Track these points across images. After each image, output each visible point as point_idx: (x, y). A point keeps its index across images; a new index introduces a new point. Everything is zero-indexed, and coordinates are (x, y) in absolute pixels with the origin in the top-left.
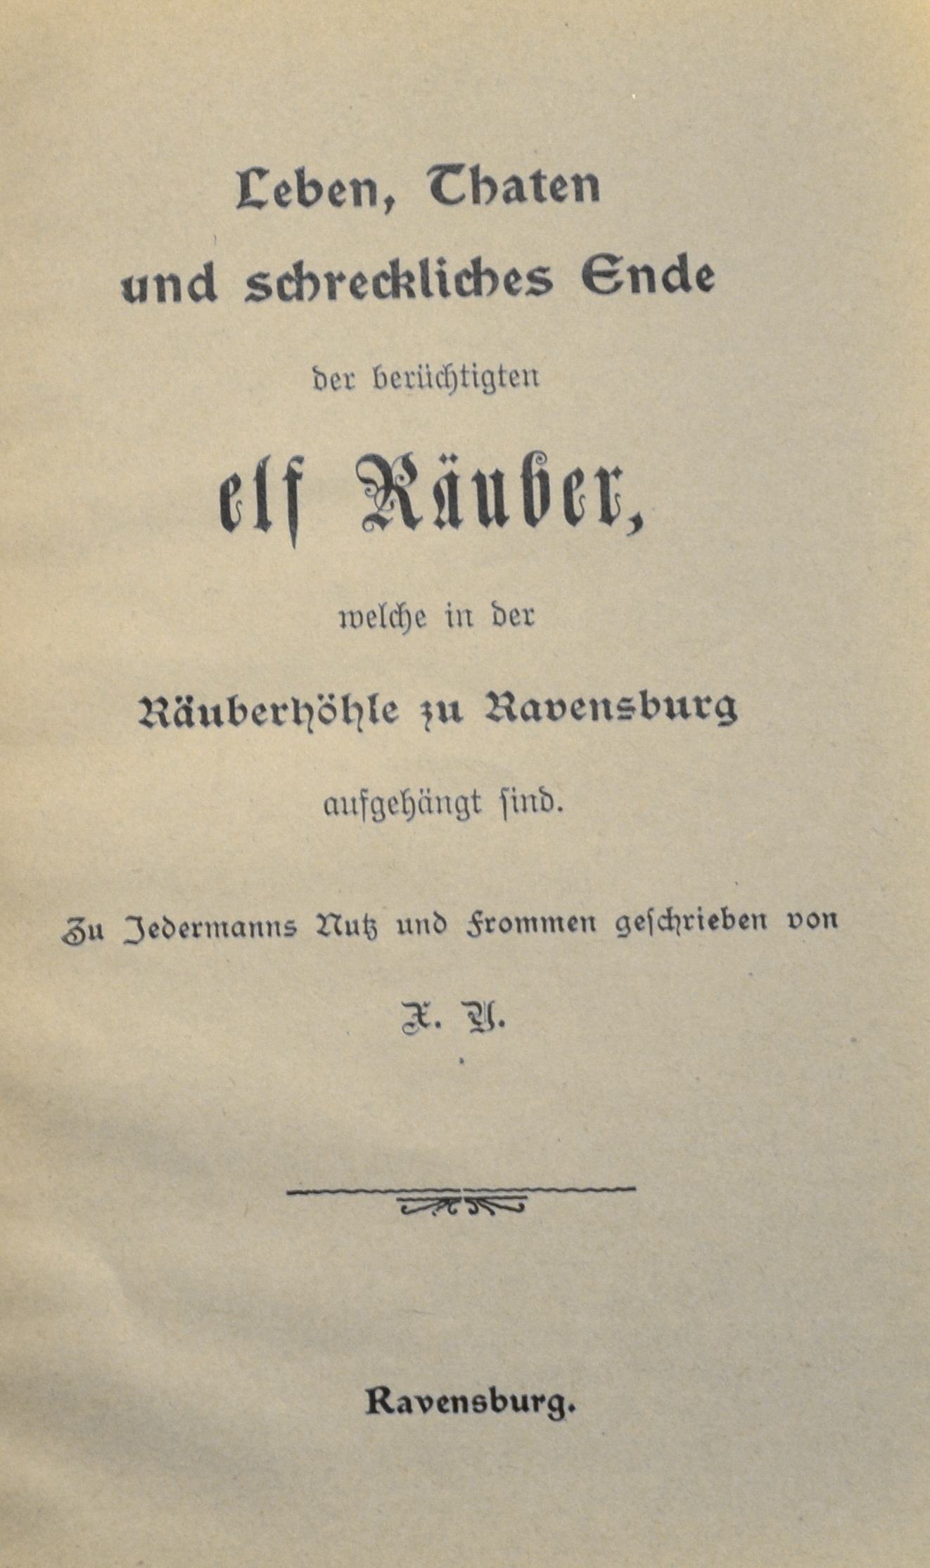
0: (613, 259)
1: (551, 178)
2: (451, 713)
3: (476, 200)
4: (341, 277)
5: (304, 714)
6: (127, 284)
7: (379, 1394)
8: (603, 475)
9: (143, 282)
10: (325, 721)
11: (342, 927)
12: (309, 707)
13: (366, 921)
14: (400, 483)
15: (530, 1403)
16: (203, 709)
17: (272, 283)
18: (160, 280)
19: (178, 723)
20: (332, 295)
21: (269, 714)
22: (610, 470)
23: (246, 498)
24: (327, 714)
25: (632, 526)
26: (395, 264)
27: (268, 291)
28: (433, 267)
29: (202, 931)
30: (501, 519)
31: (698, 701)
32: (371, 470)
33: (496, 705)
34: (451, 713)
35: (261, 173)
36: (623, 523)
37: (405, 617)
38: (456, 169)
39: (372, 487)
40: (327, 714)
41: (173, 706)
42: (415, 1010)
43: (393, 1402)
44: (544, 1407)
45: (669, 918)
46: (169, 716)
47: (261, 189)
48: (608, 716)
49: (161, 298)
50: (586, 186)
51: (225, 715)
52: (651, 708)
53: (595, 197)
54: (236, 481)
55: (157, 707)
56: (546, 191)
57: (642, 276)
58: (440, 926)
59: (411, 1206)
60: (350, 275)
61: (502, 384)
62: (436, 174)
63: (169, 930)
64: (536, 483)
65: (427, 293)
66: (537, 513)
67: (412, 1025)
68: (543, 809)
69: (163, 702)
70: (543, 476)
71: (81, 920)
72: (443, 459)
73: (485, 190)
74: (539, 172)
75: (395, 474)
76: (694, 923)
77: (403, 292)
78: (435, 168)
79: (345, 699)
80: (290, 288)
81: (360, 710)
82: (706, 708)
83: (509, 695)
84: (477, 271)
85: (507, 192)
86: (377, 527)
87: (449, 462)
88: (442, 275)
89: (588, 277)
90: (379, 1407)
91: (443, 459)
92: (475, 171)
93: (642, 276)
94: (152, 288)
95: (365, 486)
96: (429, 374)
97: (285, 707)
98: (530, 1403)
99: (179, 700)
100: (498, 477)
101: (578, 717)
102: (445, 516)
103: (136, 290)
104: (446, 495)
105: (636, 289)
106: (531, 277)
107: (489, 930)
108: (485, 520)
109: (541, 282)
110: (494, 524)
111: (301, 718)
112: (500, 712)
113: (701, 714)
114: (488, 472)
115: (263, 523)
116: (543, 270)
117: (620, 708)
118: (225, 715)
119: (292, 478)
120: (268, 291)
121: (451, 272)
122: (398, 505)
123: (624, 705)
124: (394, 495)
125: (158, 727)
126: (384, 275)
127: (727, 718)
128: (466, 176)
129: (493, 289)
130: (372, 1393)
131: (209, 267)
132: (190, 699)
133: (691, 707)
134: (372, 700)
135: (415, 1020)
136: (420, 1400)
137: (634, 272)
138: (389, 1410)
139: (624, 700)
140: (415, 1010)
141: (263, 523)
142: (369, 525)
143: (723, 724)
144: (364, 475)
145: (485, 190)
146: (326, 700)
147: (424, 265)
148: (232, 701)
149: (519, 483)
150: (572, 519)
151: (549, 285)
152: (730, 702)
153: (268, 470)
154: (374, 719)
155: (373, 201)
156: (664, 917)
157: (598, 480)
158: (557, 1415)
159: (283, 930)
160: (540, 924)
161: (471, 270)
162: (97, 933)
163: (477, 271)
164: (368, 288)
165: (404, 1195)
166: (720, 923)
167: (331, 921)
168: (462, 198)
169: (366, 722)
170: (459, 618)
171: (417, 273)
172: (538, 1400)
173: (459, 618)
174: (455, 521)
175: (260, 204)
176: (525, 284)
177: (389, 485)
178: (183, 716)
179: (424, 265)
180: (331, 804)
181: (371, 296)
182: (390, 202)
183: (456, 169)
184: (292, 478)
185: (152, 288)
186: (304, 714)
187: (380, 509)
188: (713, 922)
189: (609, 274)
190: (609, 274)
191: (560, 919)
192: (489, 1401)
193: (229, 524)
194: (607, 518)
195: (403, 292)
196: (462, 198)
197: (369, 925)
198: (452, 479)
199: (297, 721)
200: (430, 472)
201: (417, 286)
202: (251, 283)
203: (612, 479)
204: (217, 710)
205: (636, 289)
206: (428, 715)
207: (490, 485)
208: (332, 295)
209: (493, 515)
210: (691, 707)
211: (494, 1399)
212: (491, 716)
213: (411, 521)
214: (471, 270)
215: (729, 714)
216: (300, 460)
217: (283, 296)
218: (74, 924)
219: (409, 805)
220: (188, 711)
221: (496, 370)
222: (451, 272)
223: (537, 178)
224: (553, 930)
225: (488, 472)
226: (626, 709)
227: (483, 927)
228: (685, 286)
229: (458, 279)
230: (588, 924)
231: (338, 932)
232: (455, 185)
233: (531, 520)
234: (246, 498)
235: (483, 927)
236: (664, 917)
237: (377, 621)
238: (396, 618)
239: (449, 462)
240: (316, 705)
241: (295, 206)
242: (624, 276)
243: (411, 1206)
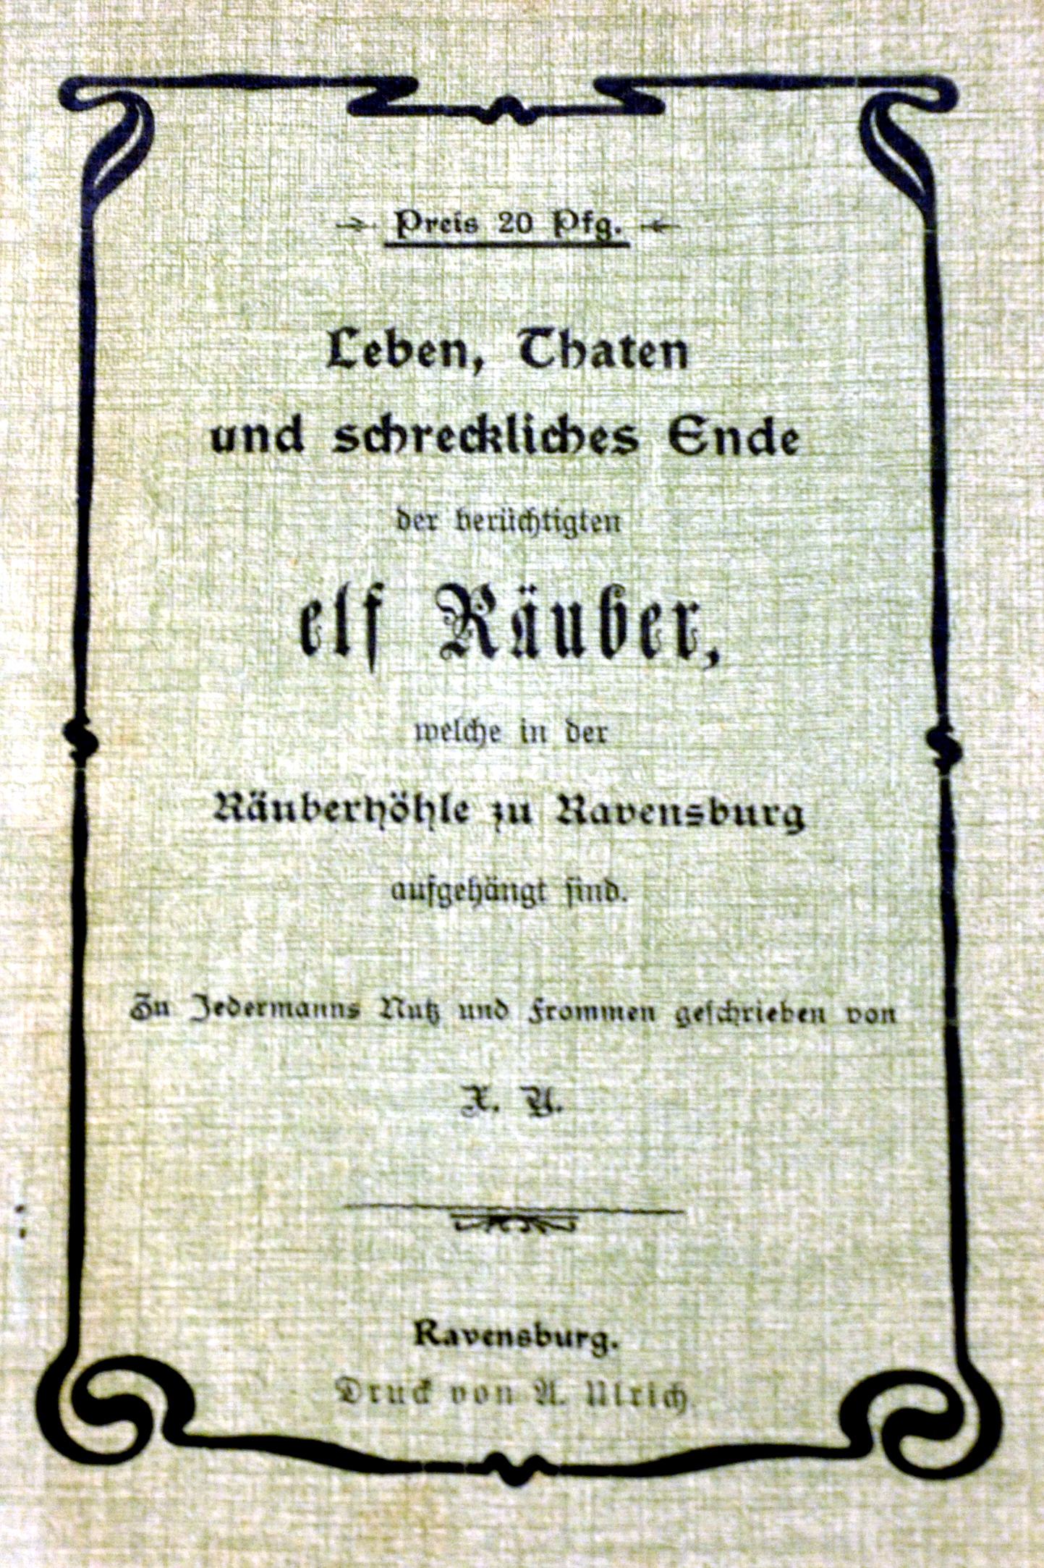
0: (699, 421)
1: (639, 344)
2: (521, 815)
3: (565, 364)
4: (429, 431)
6: (216, 434)
7: (426, 1327)
8: (681, 611)
9: (231, 433)
10: (397, 819)
11: (405, 1011)
12: (381, 805)
14: (480, 613)
15: (574, 1339)
16: (277, 805)
17: (358, 433)
18: (248, 431)
20: (419, 447)
22: (687, 605)
23: (326, 626)
24: (399, 812)
25: (708, 661)
26: (483, 419)
27: (355, 442)
28: (520, 424)
30: (578, 650)
31: (767, 809)
32: (449, 599)
34: (521, 815)
35: (352, 332)
36: (698, 657)
37: (480, 731)
38: (546, 332)
39: (450, 615)
40: (399, 812)
41: (248, 800)
42: (473, 1094)
43: (439, 1333)
44: (587, 1345)
45: (728, 1010)
46: (243, 811)
47: (352, 349)
48: (677, 822)
49: (249, 447)
50: (676, 352)
52: (720, 815)
53: (683, 364)
54: (317, 607)
55: (231, 801)
56: (634, 356)
57: (727, 439)
58: (501, 1012)
59: (464, 1222)
60: (437, 428)
61: (584, 528)
62: (523, 337)
64: (613, 617)
65: (513, 447)
66: (614, 645)
67: (470, 1108)
69: (238, 797)
70: (621, 609)
71: (147, 996)
72: (522, 590)
73: (574, 354)
74: (628, 338)
75: (473, 602)
76: (752, 1016)
77: (490, 448)
78: (524, 331)
80: (377, 441)
81: (430, 805)
82: (775, 816)
83: (580, 799)
84: (563, 427)
85: (597, 355)
86: (454, 656)
87: (528, 594)
88: (528, 432)
89: (674, 434)
90: (426, 1340)
91: (522, 590)
92: (564, 335)
93: (727, 439)
94: (240, 437)
95: (443, 614)
96: (512, 518)
97: (358, 804)
98: (574, 1339)
99: (253, 794)
100: (576, 610)
101: (647, 822)
102: (523, 645)
103: (223, 439)
104: (524, 624)
105: (721, 450)
106: (618, 436)
107: (550, 1017)
108: (562, 651)
109: (627, 441)
110: (570, 655)
112: (228, 812)
113: (769, 822)
114: (566, 604)
115: (342, 648)
116: (629, 428)
118: (298, 810)
119: (372, 604)
120: (355, 442)
121: (538, 427)
122: (475, 634)
124: (472, 625)
126: (471, 429)
127: (795, 828)
128: (556, 337)
129: (581, 362)
130: (418, 1325)
131: (297, 419)
132: (263, 794)
133: (760, 816)
134: (445, 798)
135: (473, 1103)
136: (466, 1333)
137: (719, 433)
138: (435, 1342)
139: (696, 824)
140: (473, 1094)
141: (342, 648)
142: (446, 653)
143: (791, 833)
144: (444, 604)
145: (574, 354)
146: (400, 799)
147: (511, 420)
149: (597, 615)
150: (649, 652)
151: (634, 443)
152: (798, 810)
153: (347, 599)
155: (462, 363)
157: (675, 615)
158: (599, 1351)
159: (347, 1012)
160: (600, 1013)
161: (558, 426)
162: (163, 1009)
163: (563, 427)
164: (454, 441)
165: (458, 1212)
166: (778, 1017)
167: (395, 1004)
168: (551, 360)
169: (438, 823)
170: (531, 734)
171: (504, 429)
172: (582, 1336)
173: (531, 734)
174: (532, 652)
175: (349, 364)
176: (611, 443)
177: (467, 615)
178: (256, 811)
179: (511, 420)
180: (398, 890)
181: (458, 451)
182: (479, 363)
183: (546, 332)
184: (372, 604)
185: (240, 437)
186: (376, 811)
187: (458, 637)
188: (772, 1014)
189: (696, 436)
190: (696, 436)
192: (533, 1336)
193: (309, 649)
194: (684, 652)
195: (490, 448)
196: (551, 360)
198: (530, 610)
199: (370, 818)
200: (508, 603)
201: (503, 441)
202: (339, 435)
203: (690, 615)
204: (290, 805)
205: (721, 450)
206: (499, 816)
207: (569, 644)
208: (419, 447)
209: (569, 646)
210: (760, 816)
211: (539, 1334)
213: (489, 650)
214: (558, 426)
215: (796, 824)
216: (379, 586)
217: (371, 448)
218: (141, 999)
219: (475, 893)
220: (261, 805)
221: (578, 514)
222: (538, 427)
223: (627, 344)
225: (566, 604)
226: (695, 817)
227: (544, 1014)
228: (770, 449)
229: (545, 436)
231: (401, 1015)
232: (541, 349)
233: (608, 652)
234: (326, 626)
235: (544, 1014)
237: (451, 735)
238: (470, 733)
239: (528, 594)
240: (390, 803)
241: (385, 366)
242: (710, 438)
243: (464, 1222)
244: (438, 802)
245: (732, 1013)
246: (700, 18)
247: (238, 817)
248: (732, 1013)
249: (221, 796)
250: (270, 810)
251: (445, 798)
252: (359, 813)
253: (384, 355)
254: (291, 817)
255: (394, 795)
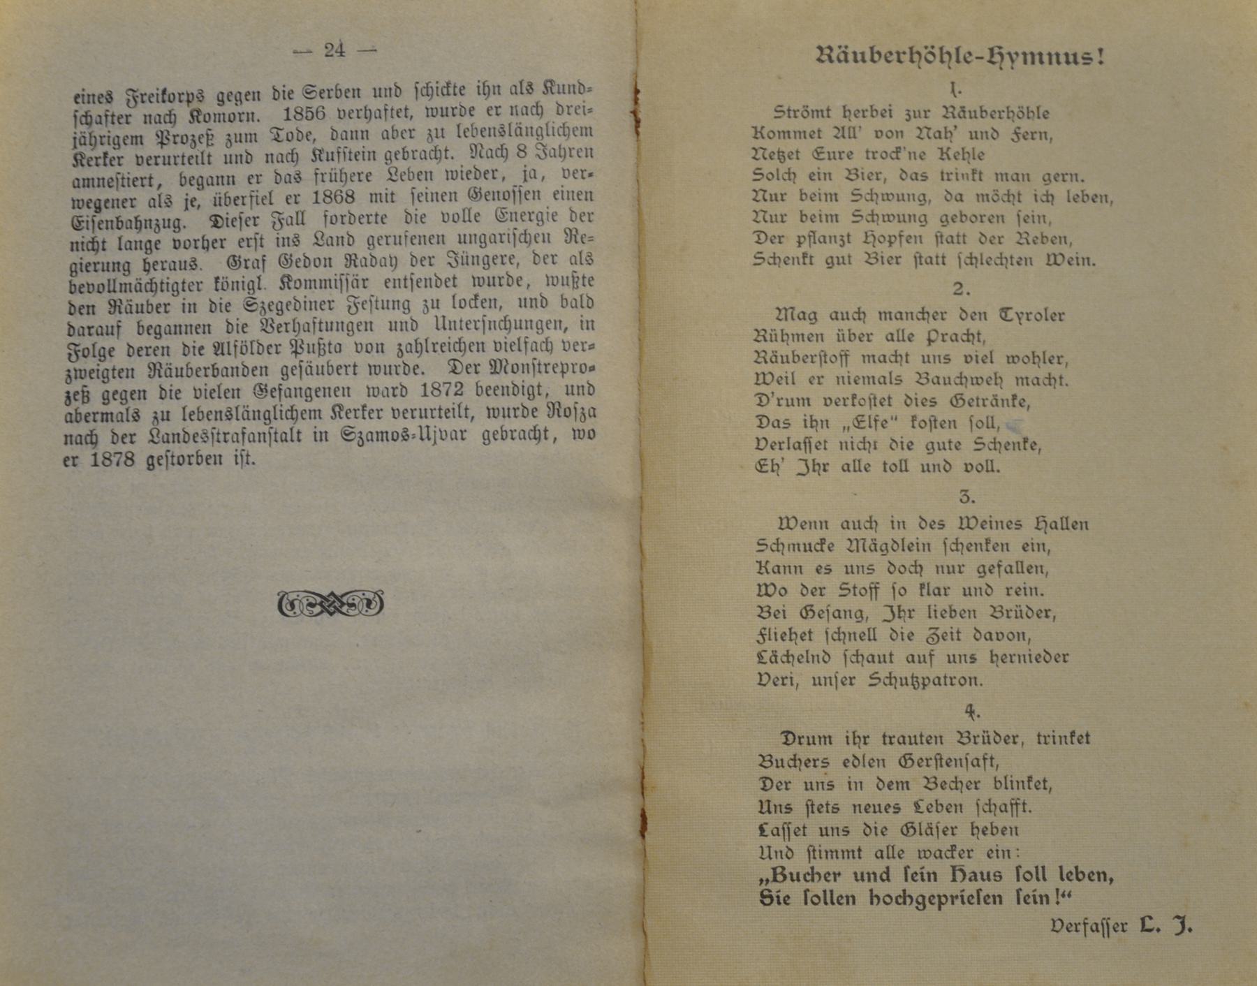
5: (916, 57)
12: (919, 53)
13: (912, 677)
16: (855, 53)
19: (839, 61)
21: (895, 57)
24: (930, 57)
29: (1016, 659)
33: (822, 54)
40: (930, 57)
45: (957, 544)
46: (834, 56)
51: (868, 57)
55: (827, 51)
63: (1048, 658)
68: (504, 199)
69: (830, 48)
71: (937, 628)
79: (941, 49)
111: (944, 59)
112: (825, 58)
117: (1083, 58)
118: (868, 57)
123: (1086, 56)
125: (827, 63)
132: (846, 47)
134: (957, 50)
146: (930, 49)
148: (872, 48)
154: (958, 61)
155: (1105, 880)
156: (835, 633)
178: (842, 57)
186: (916, 57)
191: (855, 633)
197: (915, 679)
199: (912, 61)
204: (863, 54)
212: (819, 60)
220: (845, 53)
224: (903, 789)
230: (1005, 547)
236: (835, 633)
240: (924, 52)
244: (953, 52)
245: (1071, 59)
246: (75, 133)
247: (831, 61)
248: (1071, 59)
249: (820, 48)
250: (851, 57)
251: (957, 50)
252: (905, 58)
253: (959, 219)
254: (864, 61)
255: (926, 47)
